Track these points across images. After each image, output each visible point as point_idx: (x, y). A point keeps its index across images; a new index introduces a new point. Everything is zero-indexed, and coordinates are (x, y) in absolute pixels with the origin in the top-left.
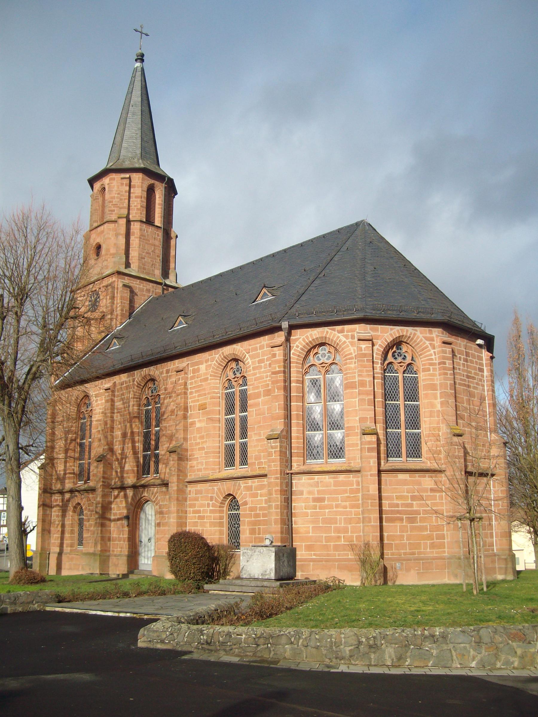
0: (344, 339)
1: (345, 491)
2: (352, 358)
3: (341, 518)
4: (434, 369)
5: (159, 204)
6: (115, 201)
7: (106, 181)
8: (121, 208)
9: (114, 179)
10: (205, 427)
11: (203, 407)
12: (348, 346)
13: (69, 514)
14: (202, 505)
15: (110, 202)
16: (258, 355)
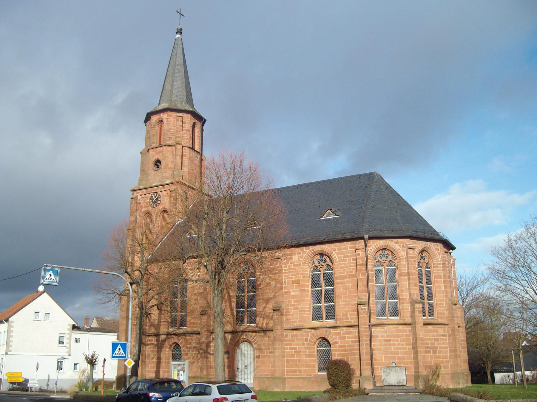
0: (398, 247)
1: (402, 336)
2: (403, 259)
3: (401, 352)
4: (440, 267)
5: (198, 136)
6: (172, 131)
7: (164, 116)
8: (177, 137)
9: (171, 116)
10: (299, 295)
11: (296, 282)
12: (400, 251)
13: (166, 350)
14: (298, 344)
15: (169, 131)
16: (343, 253)
